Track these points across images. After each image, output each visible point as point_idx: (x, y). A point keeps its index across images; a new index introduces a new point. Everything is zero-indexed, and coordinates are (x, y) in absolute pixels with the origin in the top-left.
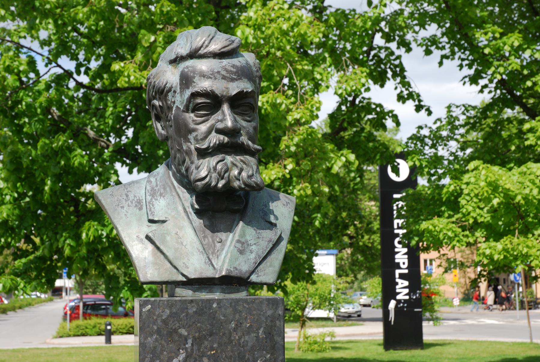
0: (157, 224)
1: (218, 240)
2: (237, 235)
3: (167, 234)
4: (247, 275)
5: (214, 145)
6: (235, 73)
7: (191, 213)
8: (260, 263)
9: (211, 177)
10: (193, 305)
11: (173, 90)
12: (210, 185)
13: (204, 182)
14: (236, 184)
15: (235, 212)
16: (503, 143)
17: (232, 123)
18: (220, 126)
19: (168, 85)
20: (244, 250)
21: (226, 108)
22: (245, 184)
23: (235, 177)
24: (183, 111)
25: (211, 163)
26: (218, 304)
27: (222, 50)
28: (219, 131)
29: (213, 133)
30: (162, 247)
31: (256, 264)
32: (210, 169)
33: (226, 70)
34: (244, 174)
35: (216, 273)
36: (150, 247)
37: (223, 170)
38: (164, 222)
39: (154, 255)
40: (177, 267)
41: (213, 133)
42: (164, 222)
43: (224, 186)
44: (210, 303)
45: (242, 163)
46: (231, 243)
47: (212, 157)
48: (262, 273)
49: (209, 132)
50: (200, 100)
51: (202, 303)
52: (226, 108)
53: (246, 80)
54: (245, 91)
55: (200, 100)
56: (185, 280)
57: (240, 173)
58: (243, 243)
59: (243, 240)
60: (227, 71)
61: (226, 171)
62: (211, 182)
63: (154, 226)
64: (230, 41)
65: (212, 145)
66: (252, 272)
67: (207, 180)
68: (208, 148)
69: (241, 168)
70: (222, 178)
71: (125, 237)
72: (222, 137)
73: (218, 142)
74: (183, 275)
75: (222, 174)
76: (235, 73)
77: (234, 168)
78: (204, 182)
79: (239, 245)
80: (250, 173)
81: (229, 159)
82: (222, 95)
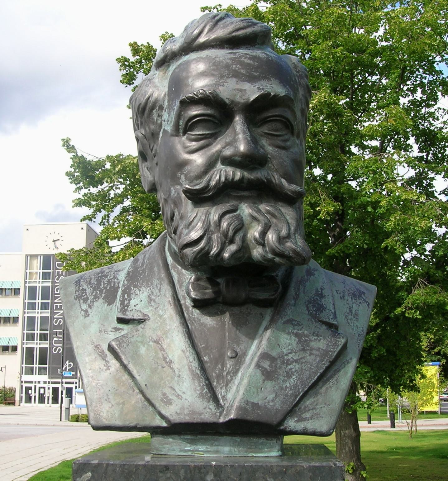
0: (130, 326)
1: (229, 354)
2: (264, 342)
3: (142, 342)
4: (279, 417)
5: (216, 183)
6: (256, 68)
7: (187, 308)
8: (305, 394)
9: (210, 240)
10: (168, 475)
11: (158, 105)
12: (208, 253)
13: (196, 249)
14: (257, 252)
15: (264, 304)
16: (360, 386)
17: (248, 143)
18: (228, 152)
19: (152, 99)
20: (275, 371)
21: (238, 120)
22: (275, 253)
23: (256, 240)
24: (172, 135)
25: (211, 217)
26: (215, 476)
27: (234, 34)
28: (229, 161)
29: (219, 166)
30: (131, 367)
31: (296, 397)
32: (209, 225)
33: (242, 64)
34: (271, 236)
35: (221, 413)
36: (114, 363)
37: (231, 228)
38: (140, 321)
39: (117, 380)
40: (153, 401)
41: (219, 166)
42: (140, 321)
43: (233, 255)
44: (200, 472)
45: (268, 216)
46: (252, 360)
47: (213, 206)
48: (308, 415)
49: (210, 165)
50: (195, 111)
51: (186, 472)
52: (238, 120)
53: (277, 82)
54: (272, 94)
55: (195, 111)
56: (164, 424)
57: (264, 234)
58: (273, 359)
59: (274, 354)
60: (241, 65)
61: (236, 231)
62: (211, 249)
63: (126, 328)
64: (248, 22)
65: (213, 183)
66: (290, 412)
67: (202, 244)
68: (206, 189)
69: (266, 224)
70: (232, 242)
71: (77, 347)
72: (230, 170)
73: (223, 179)
74: (163, 417)
75: (231, 233)
76: (256, 68)
77: (255, 224)
78: (196, 249)
79: (266, 364)
80: (284, 232)
81: (246, 210)
82: (232, 102)
